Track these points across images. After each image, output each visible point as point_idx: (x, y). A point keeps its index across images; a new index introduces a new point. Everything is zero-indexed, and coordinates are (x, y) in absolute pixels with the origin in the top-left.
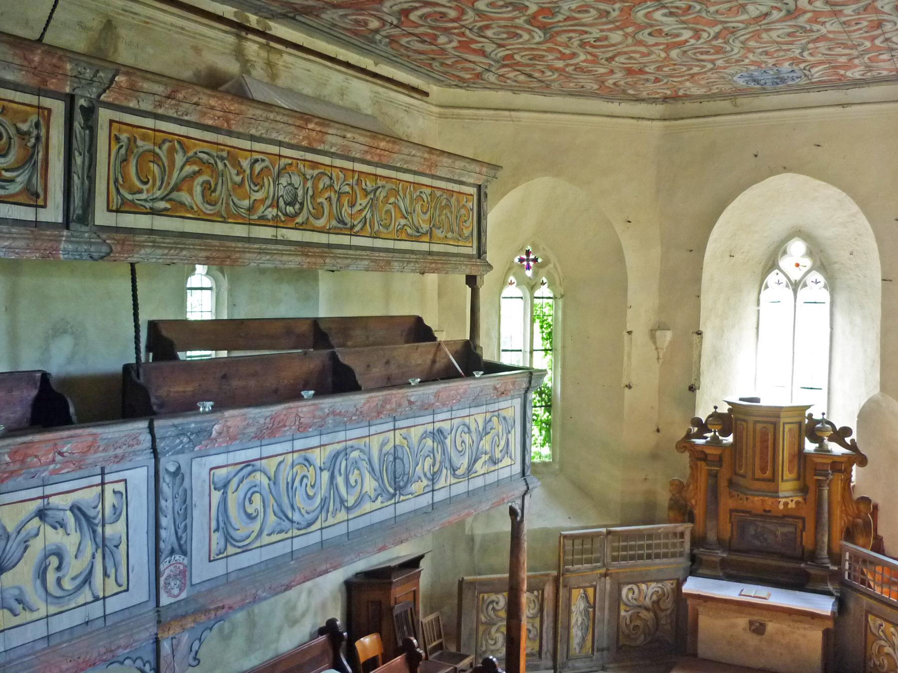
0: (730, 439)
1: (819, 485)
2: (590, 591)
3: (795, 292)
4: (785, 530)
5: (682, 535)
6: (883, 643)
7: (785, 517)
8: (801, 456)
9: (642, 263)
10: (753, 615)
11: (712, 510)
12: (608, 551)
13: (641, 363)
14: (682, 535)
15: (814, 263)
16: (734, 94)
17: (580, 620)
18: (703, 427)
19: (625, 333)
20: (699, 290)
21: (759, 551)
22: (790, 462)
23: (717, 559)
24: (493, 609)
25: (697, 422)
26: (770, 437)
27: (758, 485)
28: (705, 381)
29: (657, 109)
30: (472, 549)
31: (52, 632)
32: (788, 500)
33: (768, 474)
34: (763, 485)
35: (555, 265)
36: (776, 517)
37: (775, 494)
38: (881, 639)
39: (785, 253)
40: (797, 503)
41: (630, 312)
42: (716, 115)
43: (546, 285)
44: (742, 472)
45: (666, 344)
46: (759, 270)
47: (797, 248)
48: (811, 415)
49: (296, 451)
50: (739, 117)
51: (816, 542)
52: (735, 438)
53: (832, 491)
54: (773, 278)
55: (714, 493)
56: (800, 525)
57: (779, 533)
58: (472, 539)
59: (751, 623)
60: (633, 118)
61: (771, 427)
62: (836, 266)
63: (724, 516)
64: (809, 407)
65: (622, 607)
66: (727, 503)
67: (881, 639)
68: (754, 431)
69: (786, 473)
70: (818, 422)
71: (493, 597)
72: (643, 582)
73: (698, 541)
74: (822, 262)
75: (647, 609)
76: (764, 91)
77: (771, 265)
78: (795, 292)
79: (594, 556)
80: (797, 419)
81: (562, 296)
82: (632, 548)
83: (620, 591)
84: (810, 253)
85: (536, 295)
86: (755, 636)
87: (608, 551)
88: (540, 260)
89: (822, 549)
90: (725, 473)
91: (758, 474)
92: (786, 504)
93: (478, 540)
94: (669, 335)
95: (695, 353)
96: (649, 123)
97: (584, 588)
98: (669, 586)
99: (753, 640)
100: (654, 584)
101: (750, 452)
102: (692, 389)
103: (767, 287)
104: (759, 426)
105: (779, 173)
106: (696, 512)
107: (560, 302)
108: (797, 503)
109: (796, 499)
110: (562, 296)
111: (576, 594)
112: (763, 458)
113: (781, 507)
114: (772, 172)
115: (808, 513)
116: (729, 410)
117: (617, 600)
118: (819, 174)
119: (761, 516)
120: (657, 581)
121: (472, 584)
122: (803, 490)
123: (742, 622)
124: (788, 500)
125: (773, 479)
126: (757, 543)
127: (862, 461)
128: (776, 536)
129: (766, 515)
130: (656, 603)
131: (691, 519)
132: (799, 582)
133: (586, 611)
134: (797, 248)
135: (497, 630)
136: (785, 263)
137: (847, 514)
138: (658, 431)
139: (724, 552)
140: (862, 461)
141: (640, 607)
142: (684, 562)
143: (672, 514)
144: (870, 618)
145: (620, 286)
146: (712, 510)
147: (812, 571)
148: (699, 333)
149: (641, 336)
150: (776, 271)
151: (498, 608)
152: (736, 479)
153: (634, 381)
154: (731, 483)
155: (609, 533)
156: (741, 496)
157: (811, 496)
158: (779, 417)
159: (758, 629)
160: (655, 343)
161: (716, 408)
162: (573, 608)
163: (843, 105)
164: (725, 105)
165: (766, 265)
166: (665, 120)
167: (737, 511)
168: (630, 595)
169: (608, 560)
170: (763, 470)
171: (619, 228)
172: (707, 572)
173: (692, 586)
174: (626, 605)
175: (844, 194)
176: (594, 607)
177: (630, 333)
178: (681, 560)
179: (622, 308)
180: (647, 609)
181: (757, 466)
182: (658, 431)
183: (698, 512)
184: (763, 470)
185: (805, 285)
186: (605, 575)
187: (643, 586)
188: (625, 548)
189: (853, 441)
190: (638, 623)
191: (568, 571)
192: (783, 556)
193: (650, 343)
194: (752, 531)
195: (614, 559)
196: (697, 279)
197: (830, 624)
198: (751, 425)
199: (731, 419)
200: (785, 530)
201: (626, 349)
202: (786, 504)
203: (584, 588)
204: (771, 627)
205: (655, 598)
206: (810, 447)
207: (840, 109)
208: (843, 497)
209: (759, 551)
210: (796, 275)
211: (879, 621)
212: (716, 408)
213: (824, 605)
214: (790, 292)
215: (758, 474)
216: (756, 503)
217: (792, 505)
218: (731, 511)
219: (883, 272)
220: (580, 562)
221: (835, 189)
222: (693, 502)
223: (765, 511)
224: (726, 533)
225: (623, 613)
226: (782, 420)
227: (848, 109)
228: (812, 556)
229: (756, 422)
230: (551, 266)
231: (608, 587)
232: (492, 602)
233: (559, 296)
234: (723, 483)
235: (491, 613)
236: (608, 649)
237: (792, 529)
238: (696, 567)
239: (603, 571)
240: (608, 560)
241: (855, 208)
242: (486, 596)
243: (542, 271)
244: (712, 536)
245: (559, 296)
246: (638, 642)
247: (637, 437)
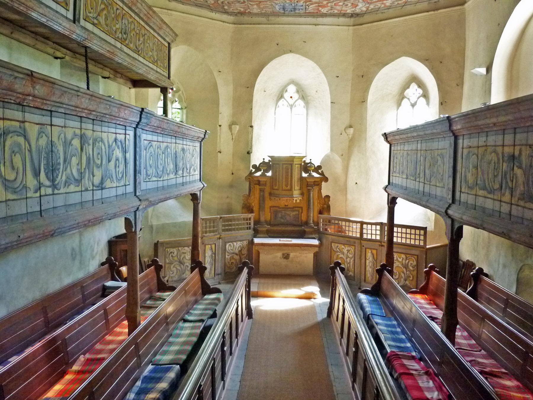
0: (269, 174)
1: (309, 191)
2: (213, 246)
3: (291, 108)
4: (294, 213)
5: (250, 219)
6: (339, 253)
7: (294, 208)
8: (302, 179)
9: (225, 92)
10: (285, 250)
11: (261, 207)
12: (220, 226)
13: (225, 141)
14: (250, 219)
15: (300, 96)
16: (266, 15)
17: (209, 260)
18: (257, 169)
19: (218, 126)
20: (252, 106)
21: (282, 224)
22: (298, 181)
23: (265, 229)
24: (172, 256)
25: (254, 166)
26: (290, 170)
27: (284, 193)
28: (254, 149)
29: (231, 18)
30: (152, 232)
31: (83, 201)
32: (297, 199)
33: (289, 187)
34: (287, 193)
35: (182, 92)
36: (290, 208)
37: (292, 196)
38: (337, 252)
39: (286, 91)
40: (300, 200)
41: (220, 116)
42: (259, 24)
43: (177, 102)
44: (276, 188)
45: (236, 132)
46: (275, 98)
47: (292, 89)
48: (305, 161)
49: (24, 199)
50: (270, 26)
51: (308, 216)
52: (272, 172)
53: (314, 194)
54: (281, 102)
55: (262, 200)
56: (301, 210)
57: (291, 215)
58: (152, 227)
59: (283, 254)
60: (221, 21)
61: (290, 167)
62: (309, 98)
63: (267, 209)
64: (304, 157)
65: (227, 254)
66: (269, 203)
67: (337, 252)
68: (283, 168)
69: (296, 186)
70: (308, 163)
71: (172, 250)
72: (235, 242)
73: (257, 222)
74: (303, 95)
75: (237, 254)
76: (284, 15)
77: (281, 96)
78: (291, 108)
79: (215, 229)
80: (300, 163)
81: (186, 108)
82: (230, 225)
83: (225, 246)
84: (298, 92)
85: (173, 107)
86: (285, 260)
87: (220, 226)
88: (174, 89)
89: (310, 220)
90: (267, 189)
91: (284, 187)
92: (296, 200)
93: (154, 228)
94: (238, 127)
95: (250, 136)
96: (228, 25)
97: (211, 244)
98: (245, 243)
99: (284, 262)
100: (239, 243)
101: (281, 178)
102: (249, 153)
103: (278, 107)
104: (285, 166)
105: (288, 53)
106: (254, 209)
107: (185, 111)
108: (300, 200)
109: (300, 198)
110: (186, 108)
111: (208, 247)
112: (287, 178)
113: (294, 202)
114: (285, 53)
115: (304, 206)
116: (269, 160)
117: (224, 250)
118: (305, 54)
119: (283, 208)
120: (240, 241)
121: (162, 243)
122: (302, 194)
123: (279, 254)
124: (297, 199)
125: (291, 190)
126: (282, 221)
127: (326, 180)
128: (290, 217)
129: (286, 208)
130: (240, 251)
131: (252, 211)
132: (302, 235)
133: (212, 256)
134: (292, 89)
135: (174, 267)
136: (286, 95)
137: (320, 203)
138: (233, 174)
139: (268, 225)
140: (326, 180)
141: (233, 253)
142: (251, 232)
143: (244, 211)
144: (333, 244)
145: (216, 103)
146: (261, 207)
147: (307, 230)
148: (252, 127)
149: (225, 128)
150: (283, 99)
151: (174, 255)
152: (273, 191)
153: (222, 150)
154: (270, 194)
155: (221, 218)
156: (277, 198)
157: (305, 197)
158: (293, 161)
159: (286, 257)
160: (231, 131)
161: (264, 159)
162: (206, 255)
163: (316, 25)
164: (263, 19)
165: (278, 97)
166: (235, 24)
167: (274, 207)
168: (230, 248)
169: (220, 231)
170: (287, 186)
171: (216, 74)
172: (262, 236)
173: (257, 241)
174: (228, 252)
175: (315, 65)
176: (215, 254)
177: (220, 126)
178: (250, 231)
179: (216, 113)
180: (237, 254)
181: (284, 183)
182: (233, 174)
183: (256, 209)
184: (287, 186)
185: (295, 106)
186: (220, 238)
187: (235, 243)
188: (228, 225)
189: (322, 171)
190: (233, 261)
191: (204, 236)
192: (294, 225)
193: (229, 131)
194: (280, 215)
195: (223, 230)
196: (250, 101)
197: (317, 249)
198: (281, 166)
199: (273, 164)
200: (294, 213)
201: (219, 134)
202: (296, 200)
203: (211, 244)
204: (292, 255)
205: (240, 249)
206: (304, 175)
207: (314, 26)
208: (318, 196)
209: (282, 224)
210: (291, 102)
211: (337, 245)
212: (264, 159)
213: (316, 242)
214: (289, 109)
215: (284, 187)
216: (283, 202)
217: (298, 201)
218: (271, 207)
219: (331, 98)
220: (210, 232)
221: (311, 62)
222: (253, 204)
223: (285, 205)
224: (268, 218)
225: (227, 257)
226: (295, 163)
227: (317, 27)
228: (306, 223)
229: (283, 164)
230: (181, 92)
231: (221, 244)
232: (171, 253)
233: (184, 108)
234: (267, 195)
235: (171, 258)
236: (221, 274)
237: (297, 213)
238: (257, 233)
239: (218, 236)
240: (220, 231)
241: (319, 71)
242: (168, 249)
243: (177, 95)
244: (262, 219)
245: (184, 108)
246: (233, 270)
247: (223, 176)
